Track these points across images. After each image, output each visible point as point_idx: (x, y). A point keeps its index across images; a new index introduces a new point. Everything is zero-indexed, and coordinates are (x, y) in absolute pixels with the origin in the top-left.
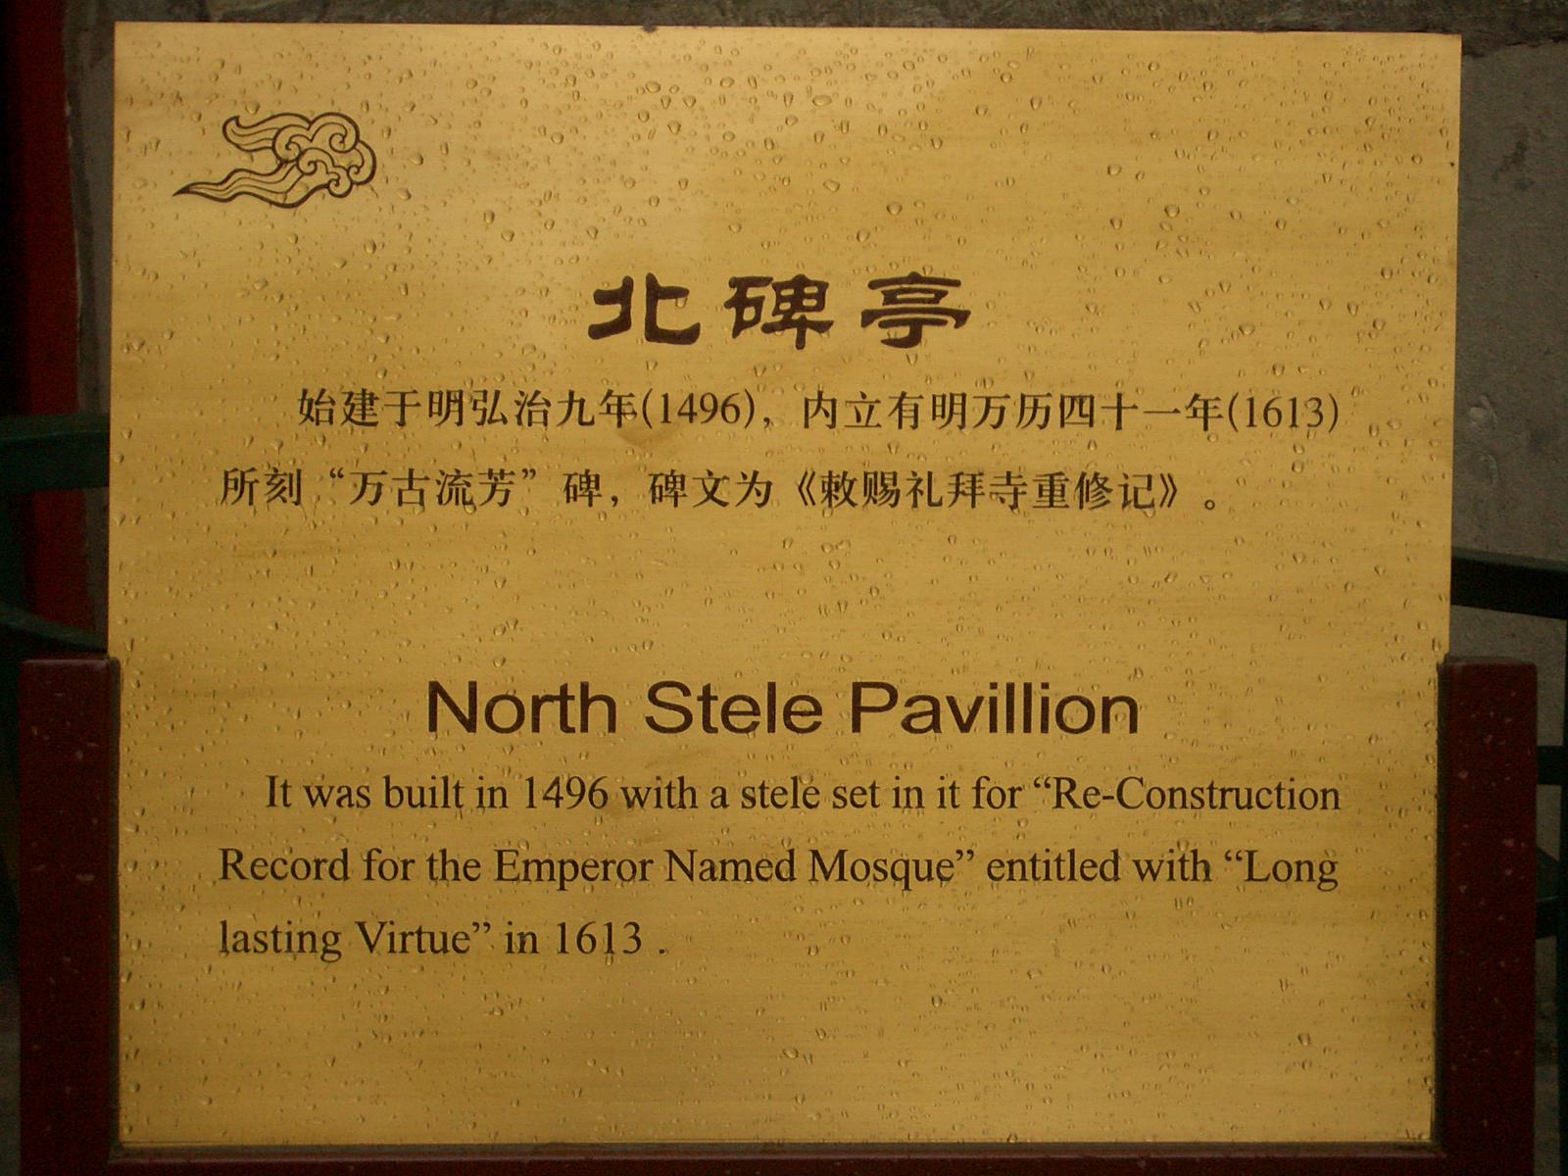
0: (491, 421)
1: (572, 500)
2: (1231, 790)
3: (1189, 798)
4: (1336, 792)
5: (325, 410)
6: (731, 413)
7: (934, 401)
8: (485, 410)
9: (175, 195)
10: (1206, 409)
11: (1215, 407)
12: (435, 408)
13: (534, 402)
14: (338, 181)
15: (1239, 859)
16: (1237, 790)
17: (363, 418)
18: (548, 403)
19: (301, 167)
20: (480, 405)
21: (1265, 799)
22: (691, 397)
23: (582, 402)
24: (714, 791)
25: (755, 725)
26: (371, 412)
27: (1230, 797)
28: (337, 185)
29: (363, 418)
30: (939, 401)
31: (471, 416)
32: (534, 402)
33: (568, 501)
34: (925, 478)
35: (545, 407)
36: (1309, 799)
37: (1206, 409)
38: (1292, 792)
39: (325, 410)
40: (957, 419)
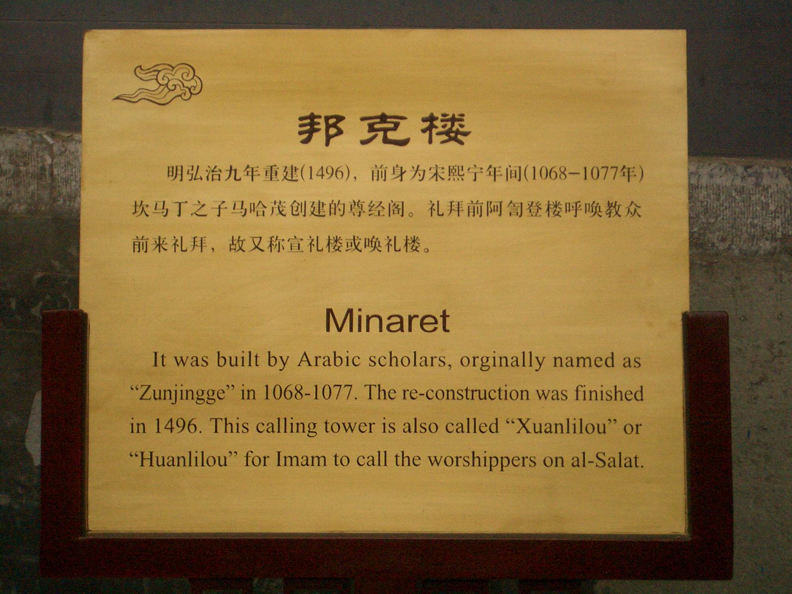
0: (195, 179)
1: (252, 211)
2: (476, 391)
3: (456, 395)
4: (480, 399)
5: (216, 174)
6: (339, 175)
7: (169, 169)
8: (192, 174)
9: (113, 99)
10: (629, 172)
11: (257, 171)
12: (171, 174)
13: (215, 170)
14: (185, 94)
15: (136, 456)
16: (479, 391)
17: (292, 178)
18: (221, 171)
19: (169, 87)
20: (190, 172)
21: (493, 395)
22: (322, 168)
23: (236, 171)
24: (624, 359)
25: (435, 329)
26: (295, 175)
27: (476, 394)
28: (185, 95)
29: (292, 178)
30: (171, 169)
31: (186, 177)
32: (215, 170)
33: (566, 212)
34: (436, 204)
35: (219, 173)
36: (514, 395)
37: (629, 172)
38: (506, 391)
39: (216, 174)
40: (179, 177)
